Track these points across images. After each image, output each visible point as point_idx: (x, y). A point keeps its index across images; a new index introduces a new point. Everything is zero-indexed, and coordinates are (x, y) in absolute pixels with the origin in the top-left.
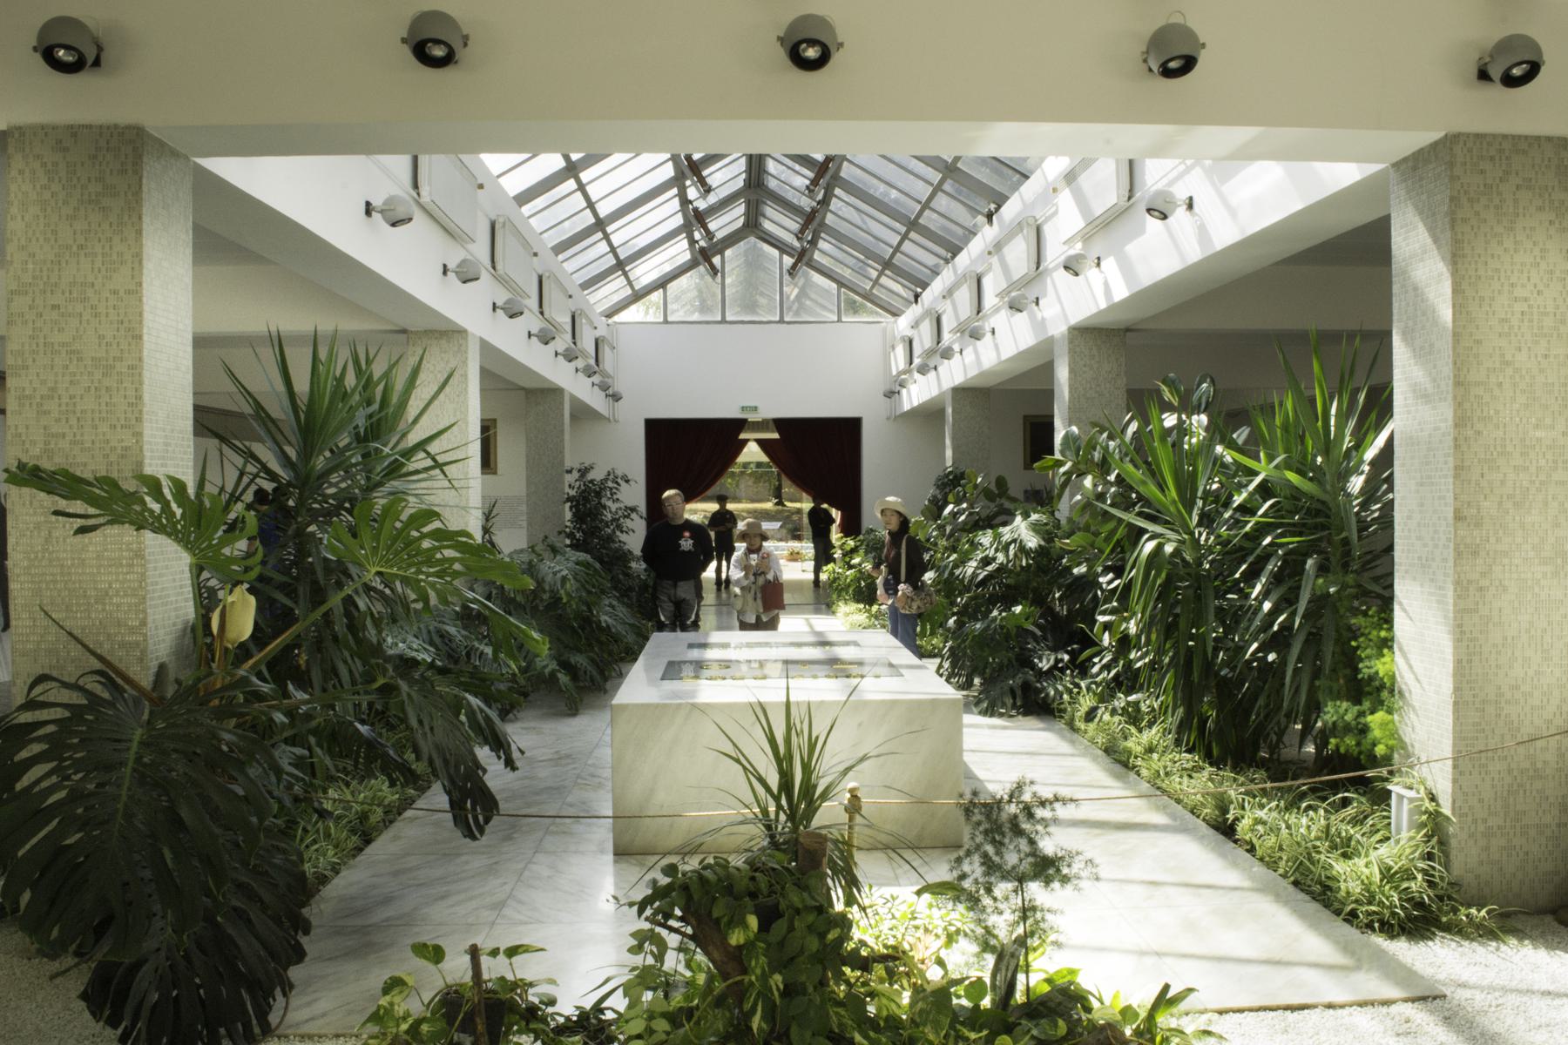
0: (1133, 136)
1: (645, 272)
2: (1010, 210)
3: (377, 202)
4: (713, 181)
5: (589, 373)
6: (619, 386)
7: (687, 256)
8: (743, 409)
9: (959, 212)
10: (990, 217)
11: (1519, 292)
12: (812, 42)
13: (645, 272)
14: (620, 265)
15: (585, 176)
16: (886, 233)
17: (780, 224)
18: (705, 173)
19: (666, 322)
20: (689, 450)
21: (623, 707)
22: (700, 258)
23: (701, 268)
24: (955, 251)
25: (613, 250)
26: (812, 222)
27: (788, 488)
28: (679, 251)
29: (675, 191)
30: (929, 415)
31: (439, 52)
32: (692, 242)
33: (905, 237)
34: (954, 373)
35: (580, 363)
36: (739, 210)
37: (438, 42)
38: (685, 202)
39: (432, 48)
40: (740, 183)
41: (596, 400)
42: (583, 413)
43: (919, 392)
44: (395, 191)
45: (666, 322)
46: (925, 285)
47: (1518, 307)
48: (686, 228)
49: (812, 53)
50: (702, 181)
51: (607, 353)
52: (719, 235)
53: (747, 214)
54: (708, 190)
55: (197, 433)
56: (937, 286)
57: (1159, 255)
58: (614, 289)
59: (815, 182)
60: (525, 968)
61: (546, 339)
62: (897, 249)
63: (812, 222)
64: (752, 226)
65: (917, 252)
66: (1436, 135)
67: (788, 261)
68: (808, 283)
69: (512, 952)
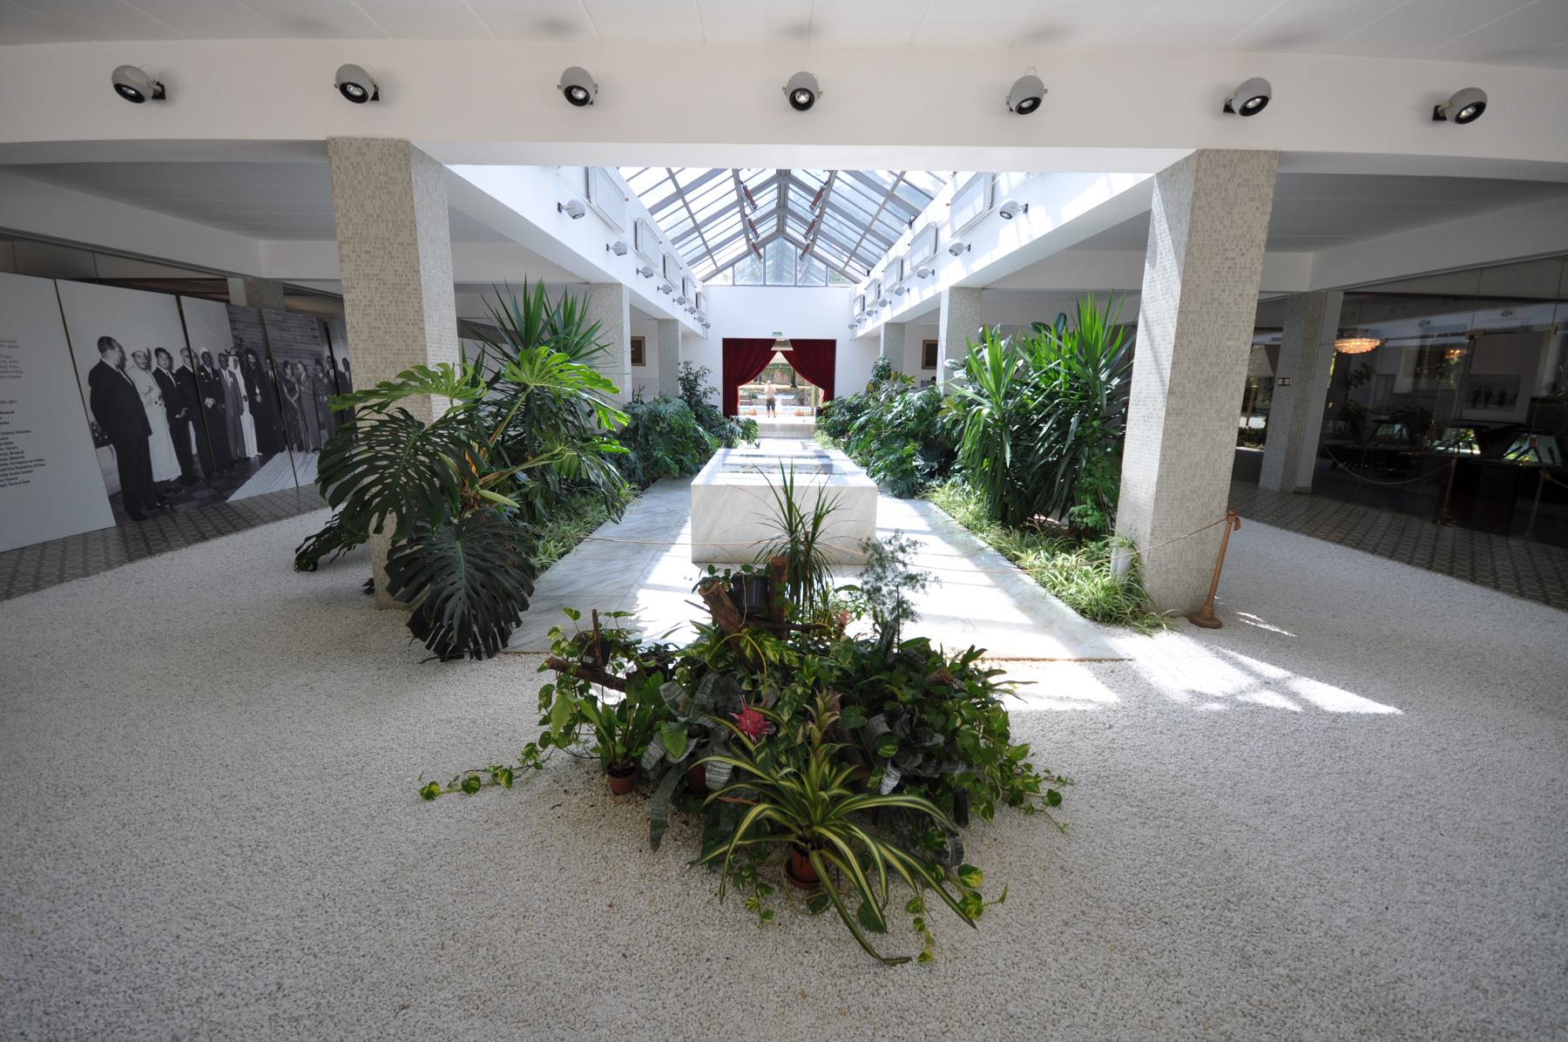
0: (994, 157)
1: (723, 257)
2: (919, 224)
3: (564, 204)
4: (759, 203)
5: (692, 311)
6: (709, 320)
7: (745, 248)
9: (895, 223)
10: (910, 224)
11: (1229, 254)
12: (804, 91)
13: (723, 257)
15: (688, 198)
16: (852, 235)
17: (795, 230)
20: (745, 358)
21: (697, 486)
24: (890, 245)
25: (705, 243)
26: (813, 228)
27: (798, 378)
28: (741, 246)
30: (872, 339)
31: (581, 95)
32: (748, 240)
33: (863, 237)
34: (887, 315)
35: (687, 306)
36: (773, 222)
38: (744, 216)
39: (576, 94)
40: (774, 205)
41: (696, 327)
42: (689, 336)
43: (870, 326)
44: (574, 197)
46: (873, 266)
47: (1227, 264)
48: (744, 232)
49: (803, 99)
50: (753, 203)
51: (702, 301)
52: (763, 236)
53: (778, 224)
56: (881, 265)
57: (1006, 242)
58: (706, 267)
59: (814, 204)
60: (622, 623)
61: (667, 290)
62: (858, 244)
63: (813, 228)
64: (781, 231)
65: (870, 246)
66: (1192, 151)
67: (800, 251)
68: (811, 264)
69: (617, 615)
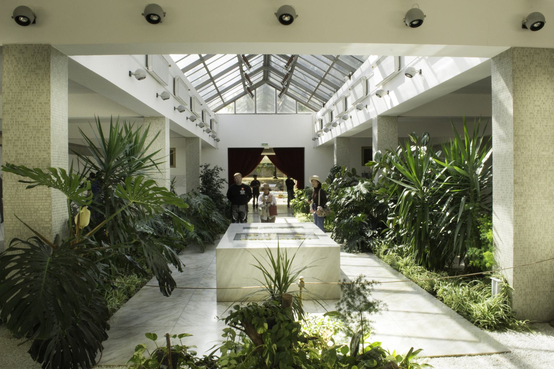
0: (400, 48)
1: (228, 96)
2: (357, 74)
3: (133, 71)
4: (252, 64)
5: (208, 132)
6: (219, 136)
7: (243, 90)
8: (263, 144)
9: (339, 75)
10: (350, 76)
11: (537, 103)
12: (287, 15)
13: (228, 96)
14: (219, 94)
15: (207, 62)
16: (313, 82)
17: (276, 79)
18: (249, 61)
19: (235, 114)
20: (243, 159)
21: (220, 250)
22: (247, 91)
23: (248, 95)
24: (337, 88)
25: (217, 88)
26: (287, 78)
27: (278, 172)
28: (240, 89)
29: (238, 67)
30: (328, 146)
31: (155, 18)
32: (245, 85)
33: (320, 84)
34: (337, 132)
35: (205, 128)
36: (261, 74)
37: (155, 15)
38: (242, 71)
39: (153, 17)
40: (261, 65)
41: (210, 141)
42: (206, 146)
43: (325, 138)
44: (140, 67)
45: (235, 114)
46: (327, 101)
47: (537, 108)
48: (243, 81)
49: (287, 19)
50: (248, 64)
51: (214, 125)
52: (254, 83)
53: (264, 76)
54: (250, 67)
55: (69, 153)
56: (331, 101)
57: (409, 90)
58: (217, 102)
59: (288, 64)
60: (186, 342)
61: (193, 120)
62: (317, 88)
63: (287, 78)
64: (266, 80)
65: (324, 89)
66: (507, 48)
67: (279, 92)
68: (286, 100)
69: (181, 336)
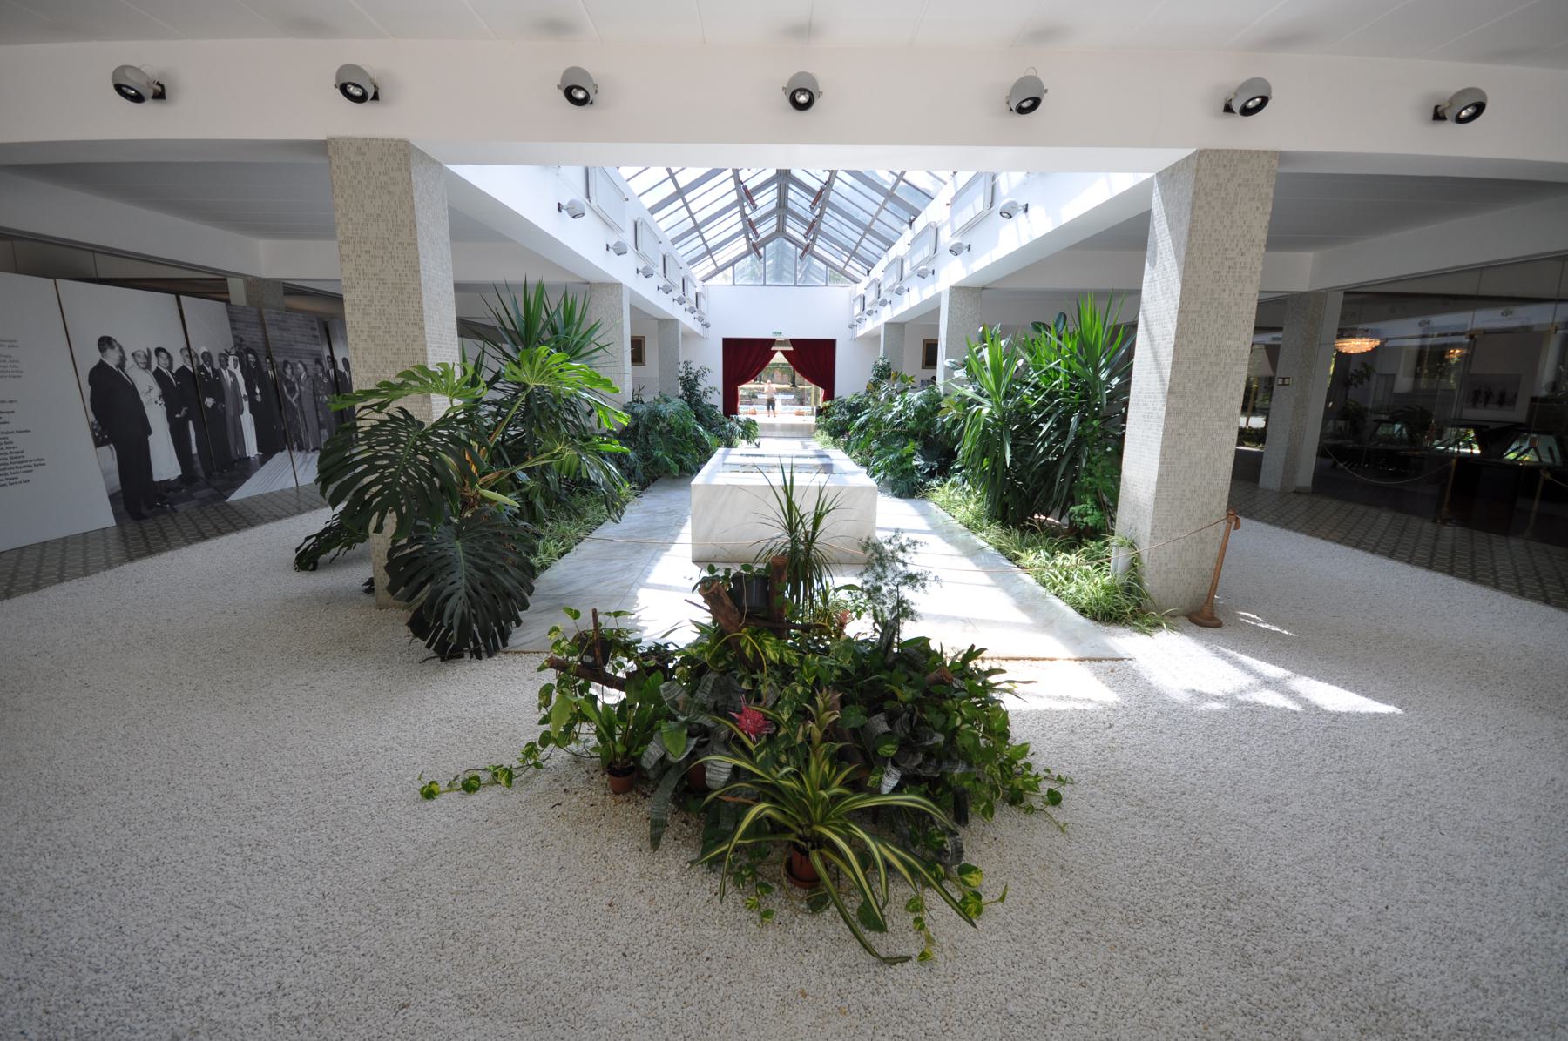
0: (994, 157)
1: (723, 257)
2: (919, 224)
3: (564, 203)
4: (759, 203)
5: (692, 311)
6: (709, 320)
7: (745, 248)
9: (895, 223)
10: (910, 223)
11: (1229, 254)
12: (804, 91)
13: (723, 257)
15: (688, 197)
16: (852, 234)
17: (795, 230)
20: (745, 358)
21: (697, 486)
24: (890, 244)
25: (705, 243)
26: (813, 227)
27: (798, 377)
28: (741, 245)
30: (872, 339)
31: (581, 95)
32: (748, 240)
33: (863, 237)
34: (887, 315)
35: (687, 305)
36: (773, 222)
38: (744, 215)
39: (576, 94)
40: (774, 205)
41: (696, 327)
42: (689, 336)
43: (870, 325)
44: (574, 197)
46: (873, 265)
47: (1227, 263)
48: (744, 231)
49: (803, 99)
50: (753, 202)
51: (702, 301)
52: (763, 236)
53: (778, 224)
55: (461, 335)
56: (881, 265)
57: (1006, 242)
58: (706, 266)
59: (814, 203)
60: (622, 623)
61: (667, 290)
62: (858, 244)
63: (813, 227)
64: (781, 231)
65: (870, 246)
66: (1192, 151)
67: (800, 251)
68: (811, 264)
69: (617, 614)
